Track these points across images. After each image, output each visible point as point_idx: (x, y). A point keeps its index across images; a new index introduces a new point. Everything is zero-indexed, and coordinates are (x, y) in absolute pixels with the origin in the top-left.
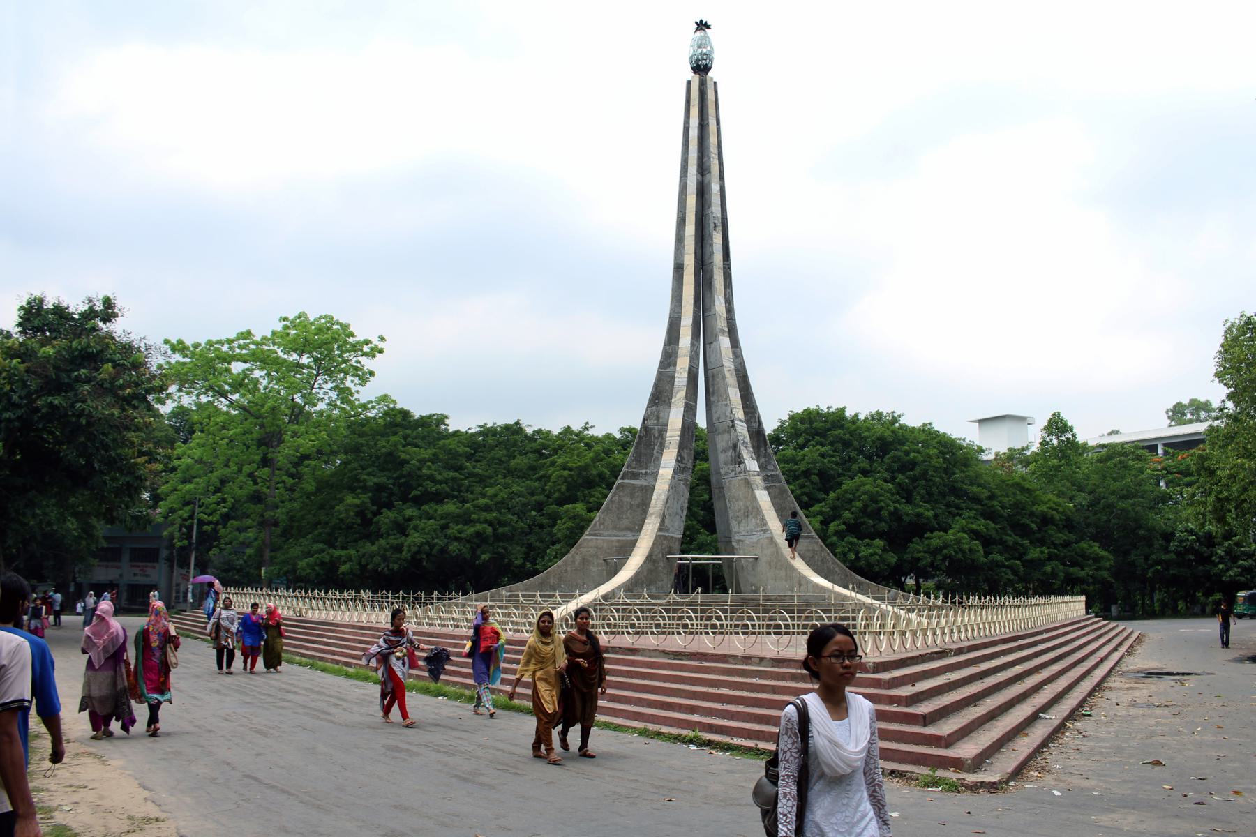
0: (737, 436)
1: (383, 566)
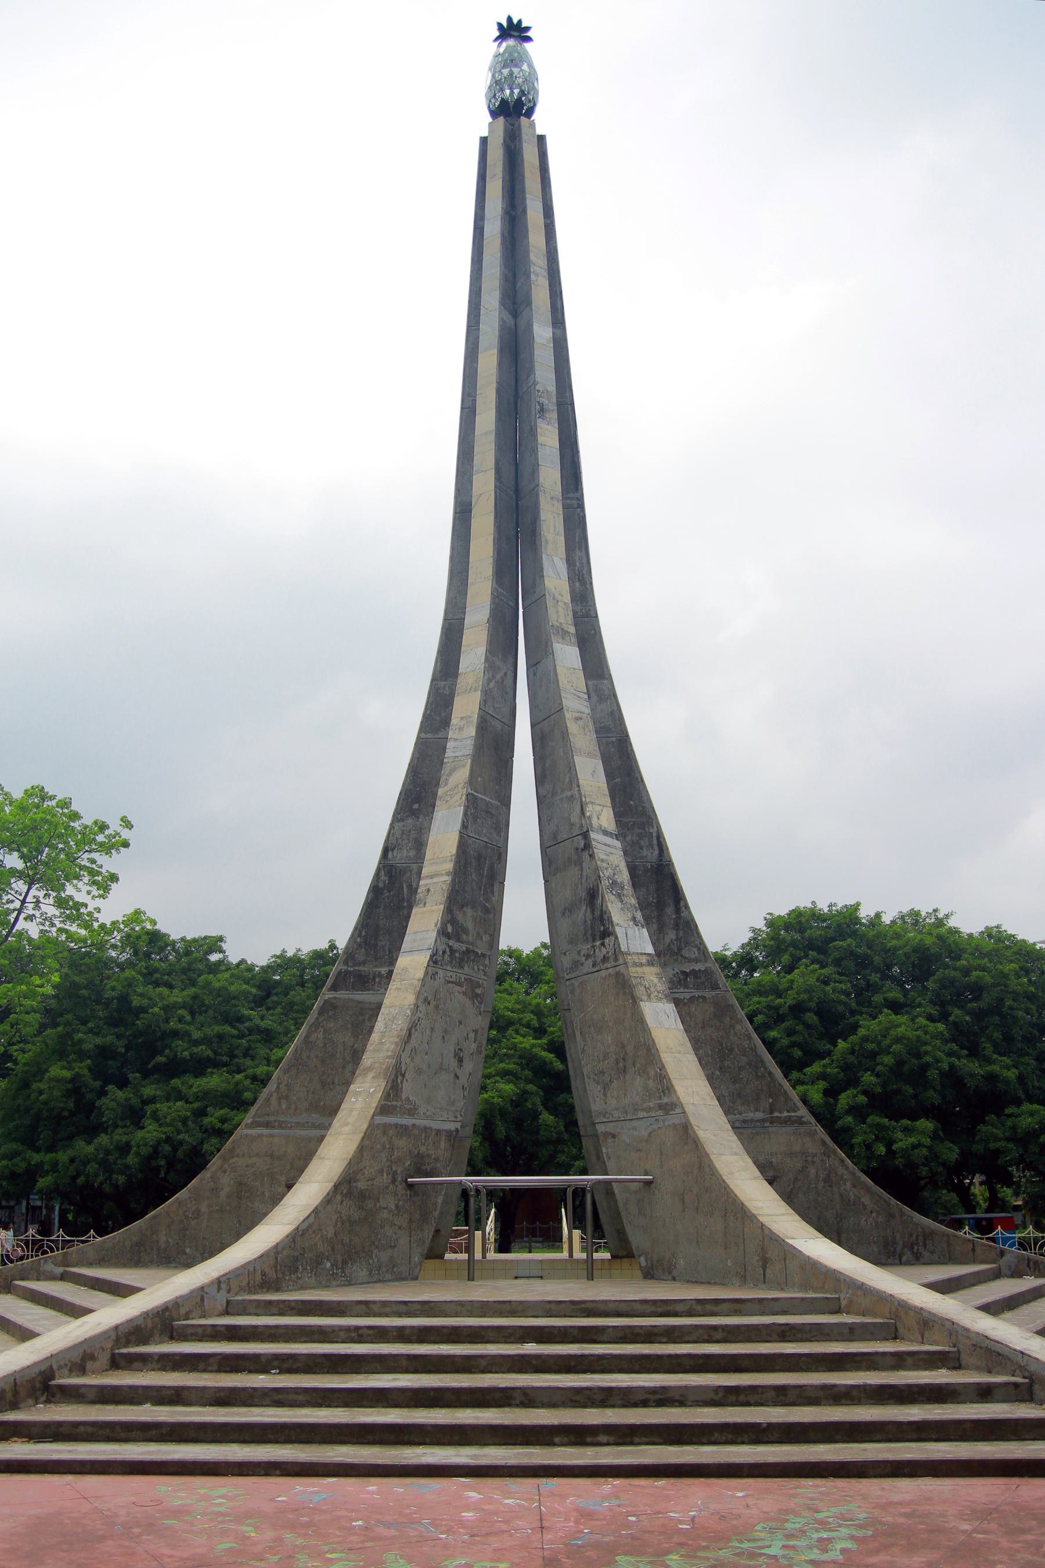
0: (597, 869)
1: (101, 1178)
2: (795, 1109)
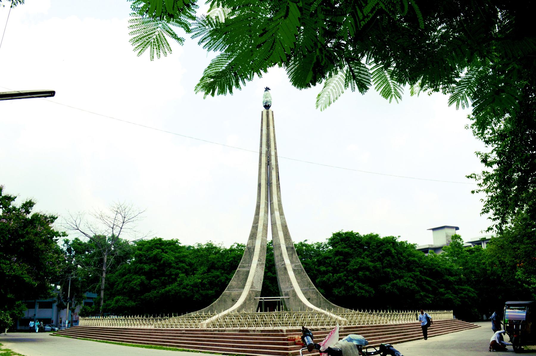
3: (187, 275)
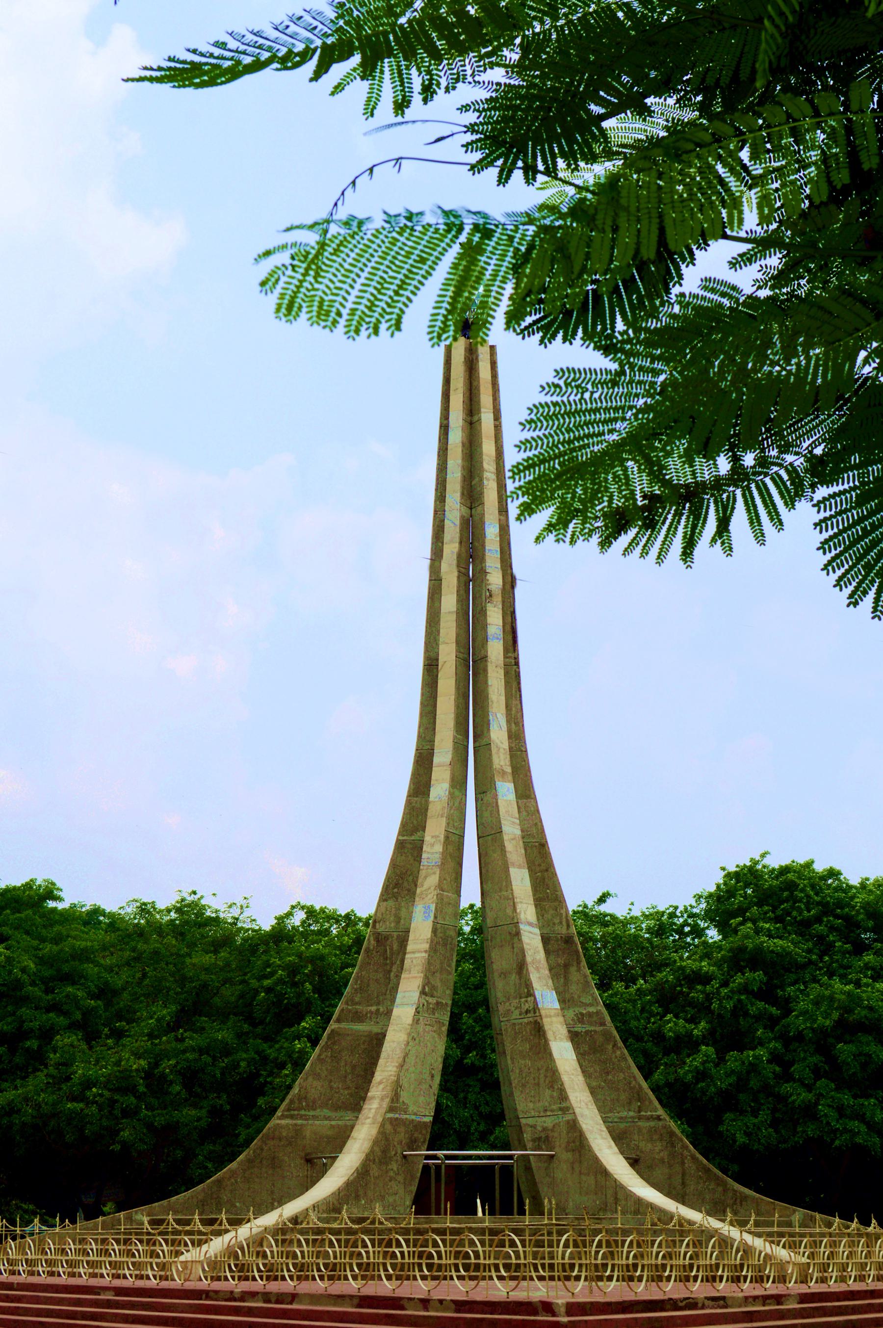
2: (656, 1110)
3: (91, 1037)
